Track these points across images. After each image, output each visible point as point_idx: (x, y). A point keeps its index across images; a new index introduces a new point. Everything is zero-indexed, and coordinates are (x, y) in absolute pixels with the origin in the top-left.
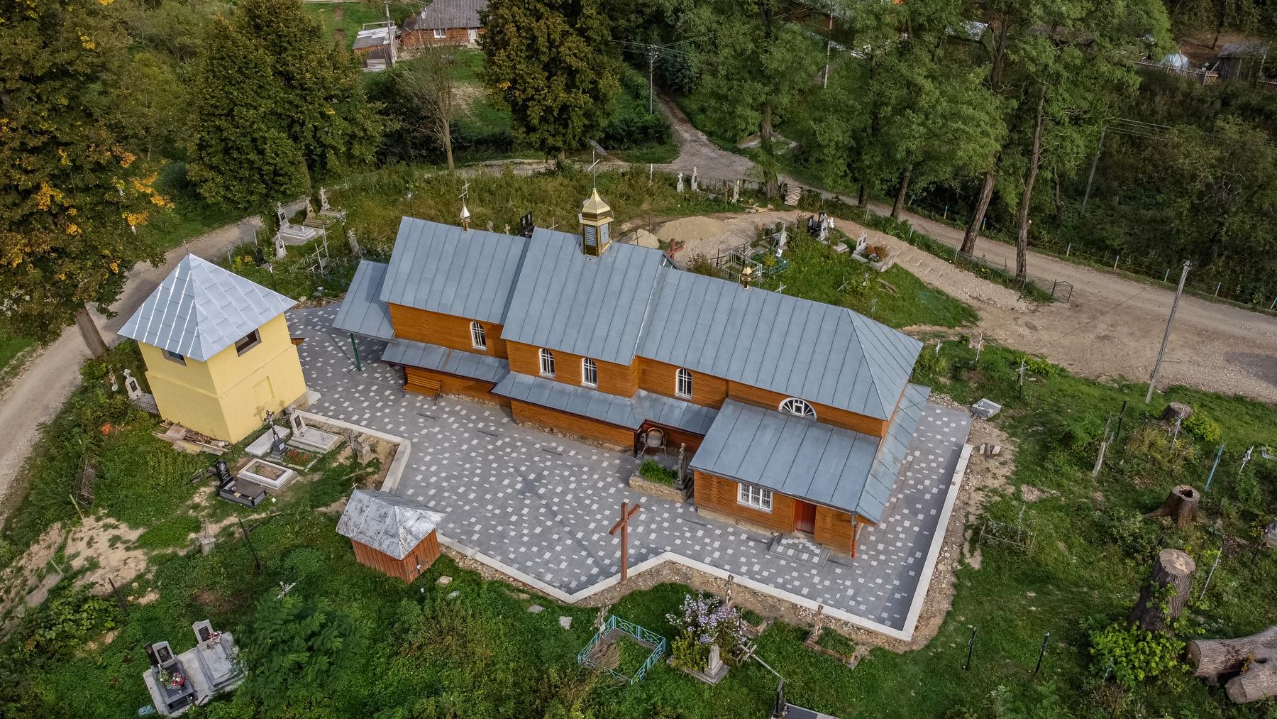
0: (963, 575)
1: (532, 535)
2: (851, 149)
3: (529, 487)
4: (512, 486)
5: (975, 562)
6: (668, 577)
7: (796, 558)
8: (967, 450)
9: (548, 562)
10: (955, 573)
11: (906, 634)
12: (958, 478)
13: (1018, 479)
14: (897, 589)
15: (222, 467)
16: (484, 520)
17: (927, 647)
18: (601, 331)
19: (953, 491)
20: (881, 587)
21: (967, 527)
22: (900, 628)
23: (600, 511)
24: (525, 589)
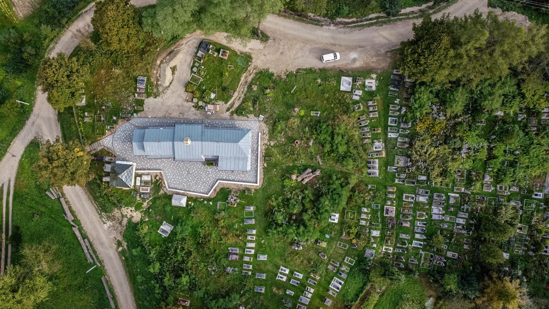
0: (264, 168)
1: (194, 183)
2: (496, 176)
3: (188, 172)
4: (185, 173)
5: (266, 165)
6: (221, 186)
7: (238, 173)
8: (260, 134)
9: (200, 188)
10: (263, 168)
11: (258, 184)
12: (259, 143)
13: (269, 141)
14: (255, 173)
15: (104, 8)
16: (185, 183)
17: (262, 186)
18: (194, 154)
19: (259, 147)
20: (252, 173)
21: (263, 156)
22: (257, 183)
23: (203, 173)
24: (201, 197)
